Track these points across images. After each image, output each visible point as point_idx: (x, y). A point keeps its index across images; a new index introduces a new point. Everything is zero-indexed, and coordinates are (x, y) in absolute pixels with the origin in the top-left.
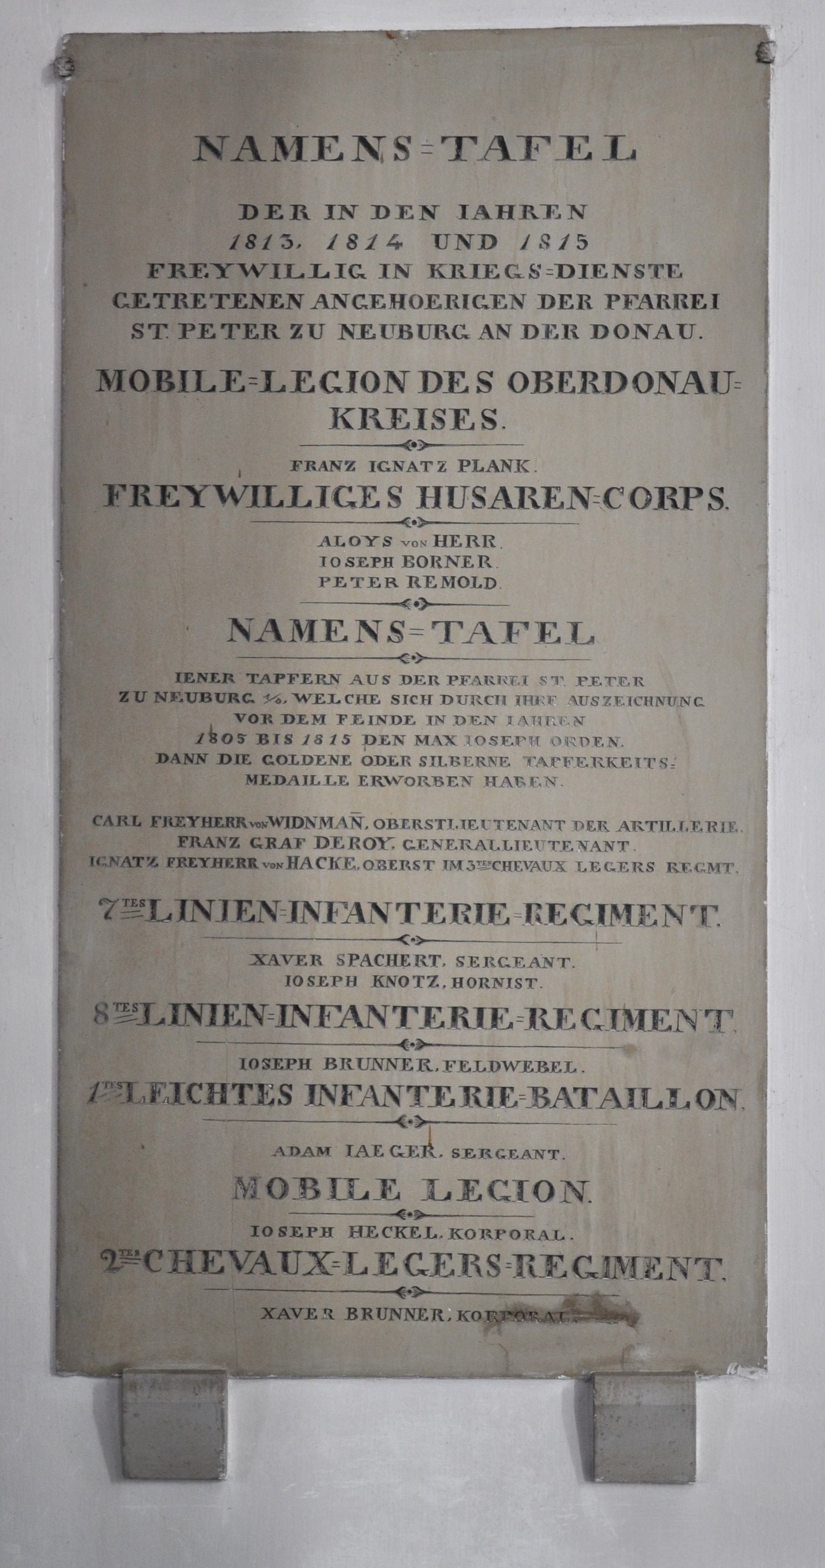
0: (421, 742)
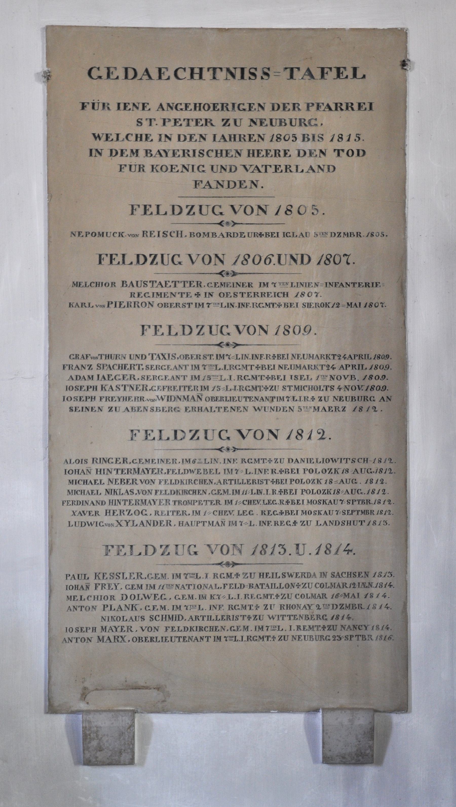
0: (316, 410)
